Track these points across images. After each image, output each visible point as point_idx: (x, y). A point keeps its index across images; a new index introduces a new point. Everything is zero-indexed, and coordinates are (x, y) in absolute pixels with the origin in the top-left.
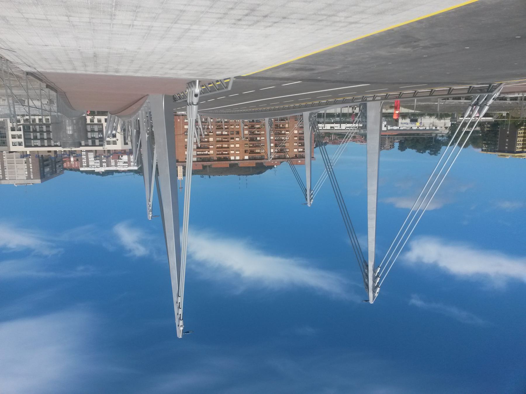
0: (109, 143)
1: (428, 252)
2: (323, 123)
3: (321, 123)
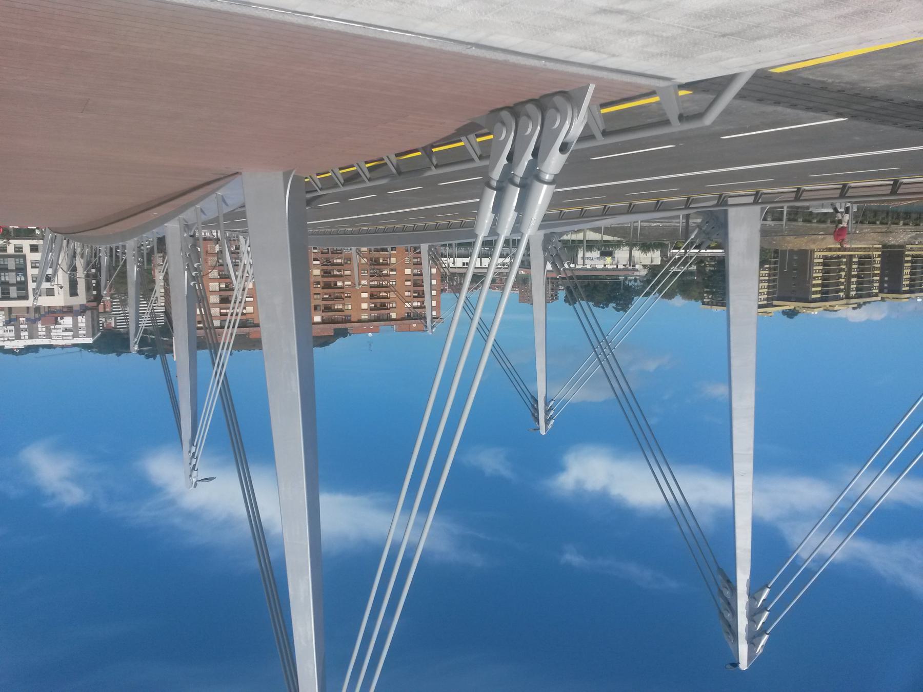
0: (37, 293)
3: (445, 257)
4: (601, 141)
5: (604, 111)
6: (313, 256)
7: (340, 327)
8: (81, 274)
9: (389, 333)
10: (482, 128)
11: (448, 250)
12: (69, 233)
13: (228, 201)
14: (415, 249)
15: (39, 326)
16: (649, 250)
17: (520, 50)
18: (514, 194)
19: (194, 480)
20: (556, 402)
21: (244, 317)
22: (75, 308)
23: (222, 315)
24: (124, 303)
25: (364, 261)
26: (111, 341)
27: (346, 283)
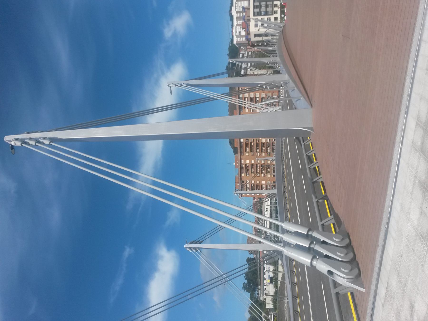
0: (256, 20)
1: (167, 263)
2: (271, 203)
4: (333, 292)
5: (349, 294)
6: (271, 139)
7: (238, 150)
8: (264, 38)
9: (235, 173)
10: (339, 228)
11: (273, 202)
12: (283, 33)
13: (298, 102)
14: (274, 186)
15: (242, 21)
16: (273, 302)
17: (385, 254)
18: (305, 244)
19: (171, 85)
20: (200, 253)
21: (244, 108)
22: (249, 36)
23: (245, 98)
24: (251, 57)
25: (269, 162)
26: (234, 51)
27: (258, 154)
